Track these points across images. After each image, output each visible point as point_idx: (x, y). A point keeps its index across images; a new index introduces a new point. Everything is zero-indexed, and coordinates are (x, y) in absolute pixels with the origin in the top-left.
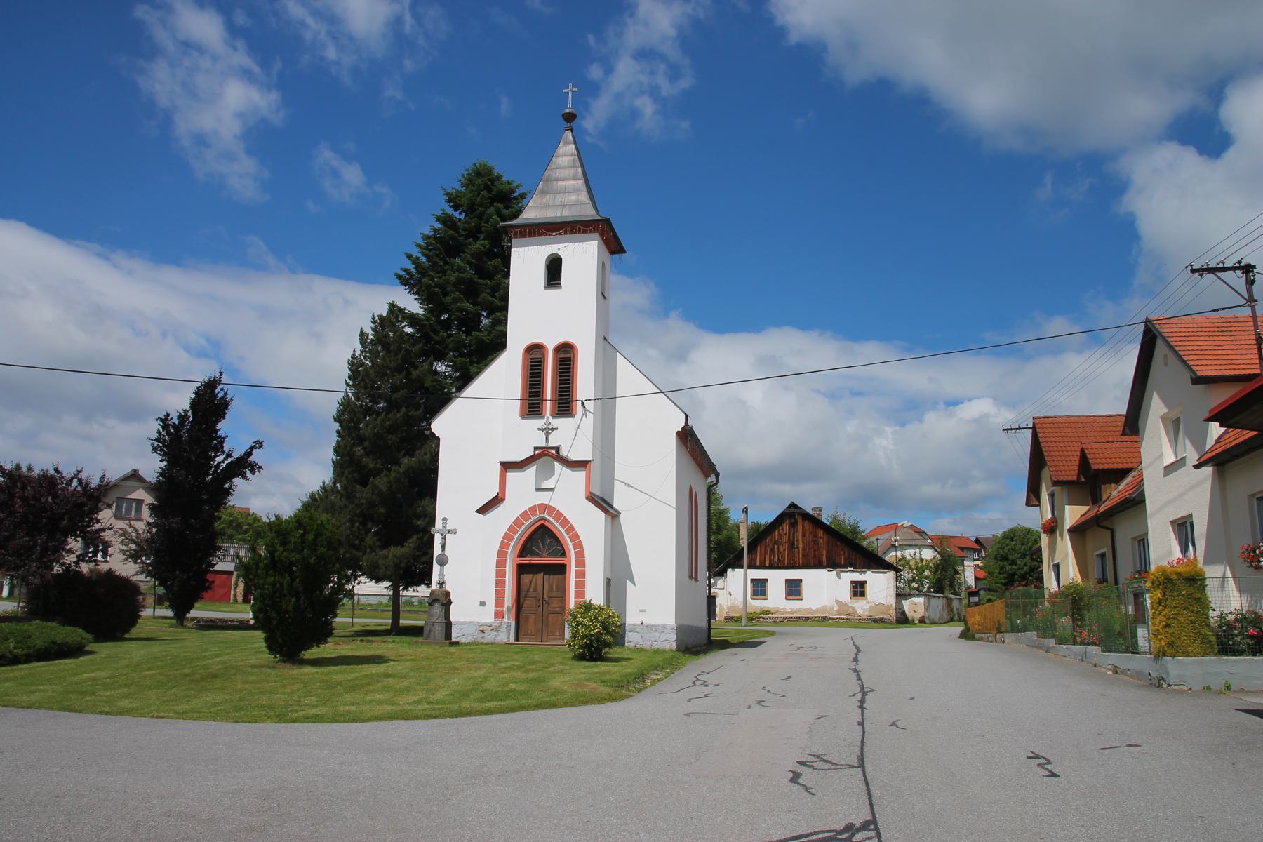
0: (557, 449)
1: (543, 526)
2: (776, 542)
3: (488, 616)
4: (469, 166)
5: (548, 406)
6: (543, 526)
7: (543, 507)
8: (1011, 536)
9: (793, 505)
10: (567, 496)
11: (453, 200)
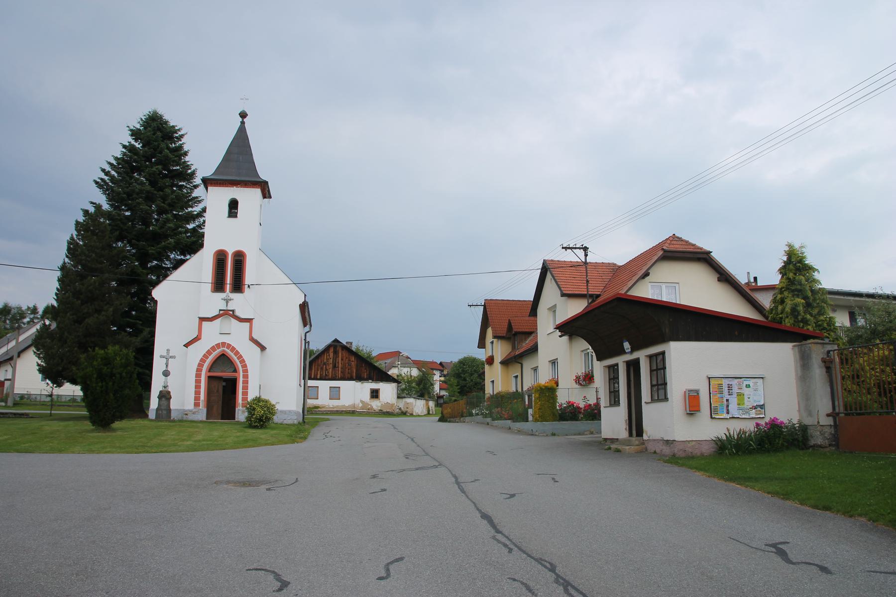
0: (233, 311)
1: (223, 355)
2: (324, 364)
3: (189, 405)
4: (146, 112)
5: (228, 287)
6: (223, 355)
7: (224, 344)
8: (464, 362)
9: (336, 341)
10: (236, 337)
11: (135, 134)
